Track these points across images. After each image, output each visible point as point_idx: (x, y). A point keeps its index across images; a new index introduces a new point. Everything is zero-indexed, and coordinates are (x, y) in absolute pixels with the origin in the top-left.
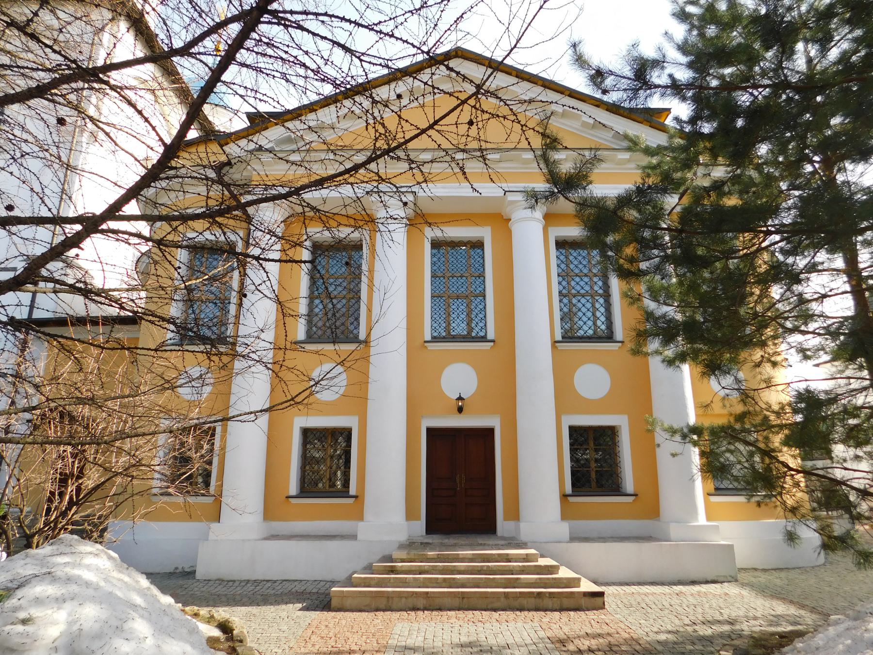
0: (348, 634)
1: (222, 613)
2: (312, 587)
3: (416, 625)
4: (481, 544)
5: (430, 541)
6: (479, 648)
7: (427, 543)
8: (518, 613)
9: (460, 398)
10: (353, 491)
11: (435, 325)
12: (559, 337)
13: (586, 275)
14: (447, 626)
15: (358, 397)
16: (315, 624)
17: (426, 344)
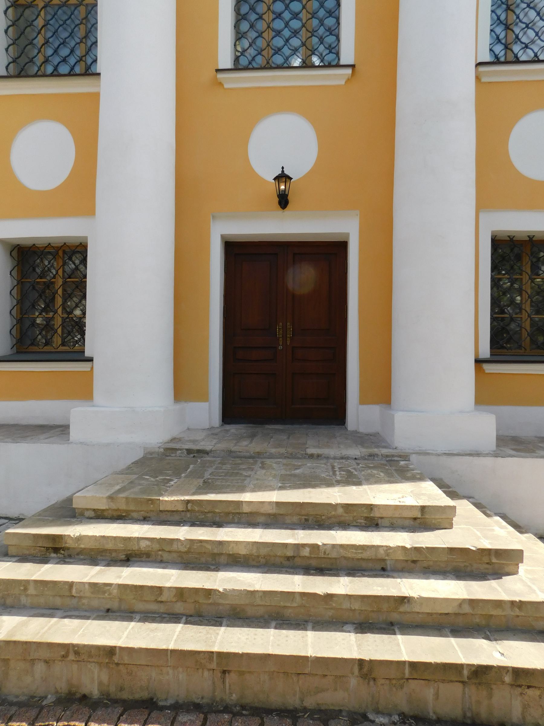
9: (283, 177)
17: (220, 76)
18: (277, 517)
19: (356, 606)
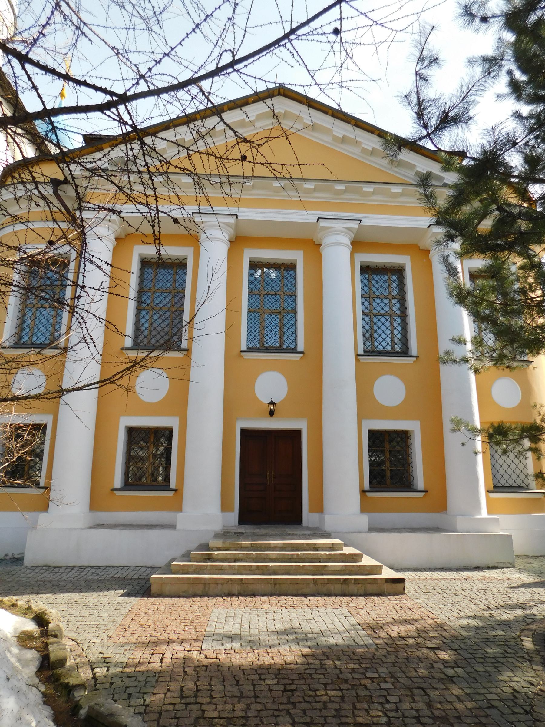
0: (167, 622)
1: (40, 602)
2: (134, 572)
3: (232, 611)
4: (289, 534)
5: (243, 531)
6: (295, 636)
7: (239, 533)
8: (326, 598)
9: (272, 403)
10: (172, 485)
11: (251, 337)
12: (361, 351)
13: (386, 298)
14: (262, 612)
15: (179, 399)
16: (135, 610)
17: (242, 354)
18: (283, 548)
19: (312, 569)
